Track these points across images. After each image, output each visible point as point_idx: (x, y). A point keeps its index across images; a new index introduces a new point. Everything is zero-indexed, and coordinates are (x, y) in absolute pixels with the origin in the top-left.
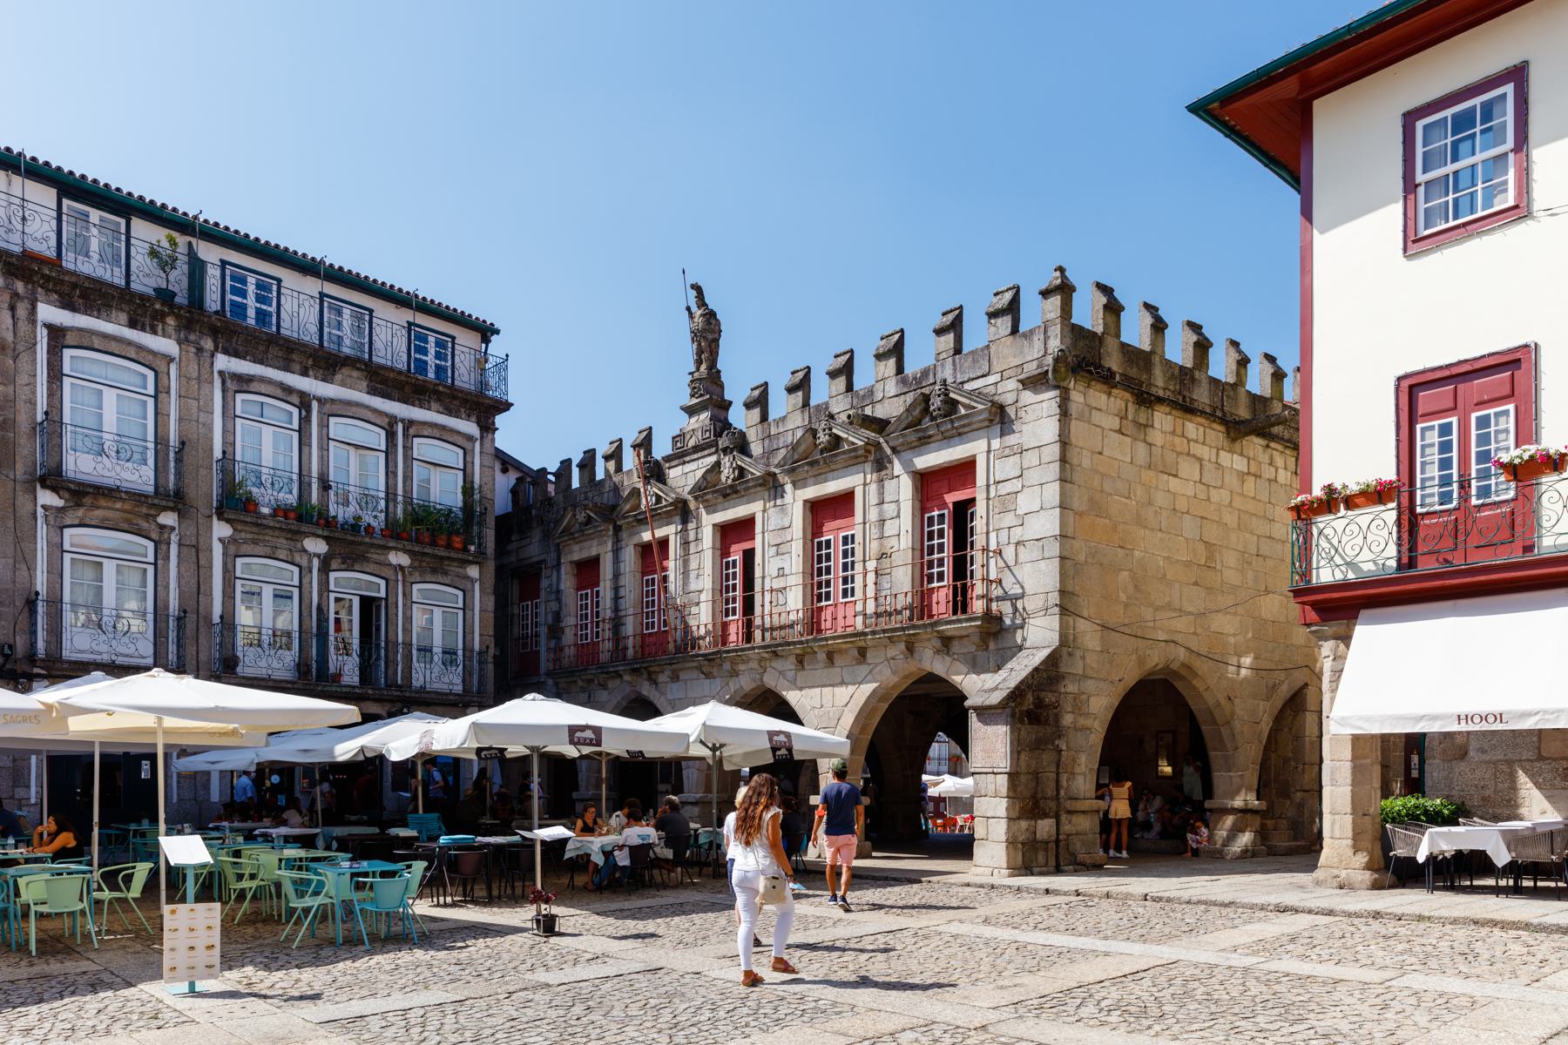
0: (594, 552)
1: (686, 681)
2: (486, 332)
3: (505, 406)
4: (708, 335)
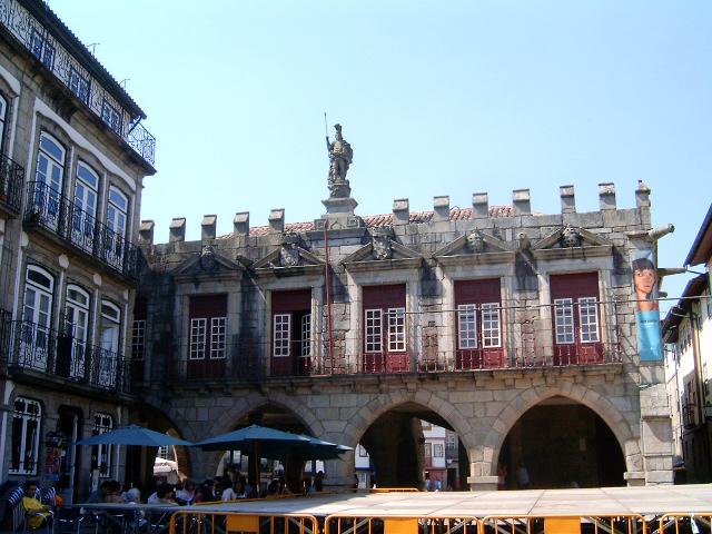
0: (220, 289)
1: (330, 395)
2: (135, 112)
3: (151, 171)
4: (342, 158)
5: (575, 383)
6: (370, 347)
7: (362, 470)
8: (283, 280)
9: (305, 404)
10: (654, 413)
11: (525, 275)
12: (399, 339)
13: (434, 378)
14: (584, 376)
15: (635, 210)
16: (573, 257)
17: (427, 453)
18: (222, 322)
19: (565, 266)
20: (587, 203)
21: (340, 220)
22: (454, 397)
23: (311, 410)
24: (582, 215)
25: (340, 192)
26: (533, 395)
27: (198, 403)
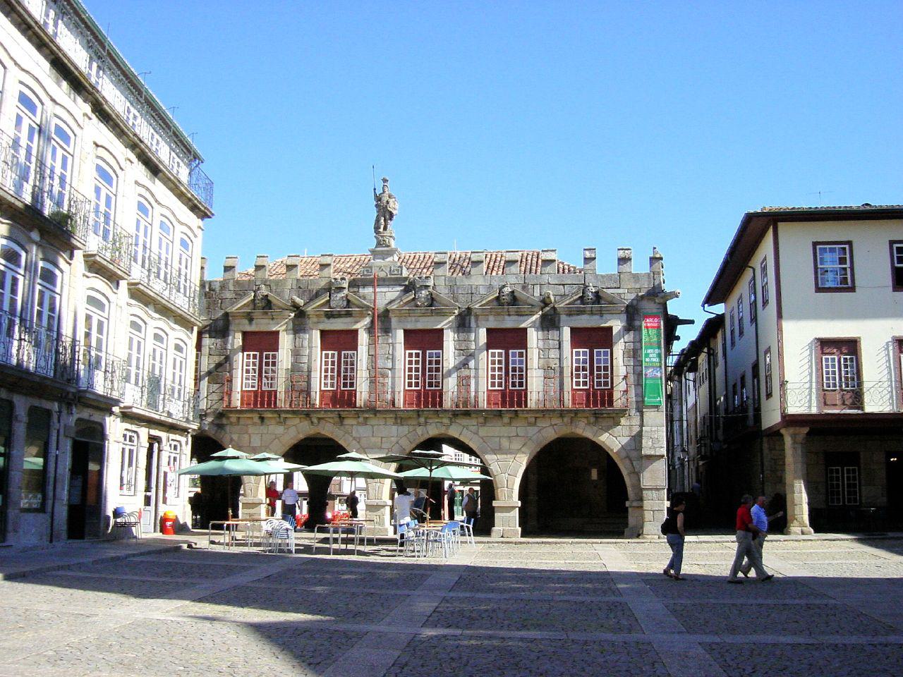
5: (589, 424)
6: (431, 385)
7: (301, 494)
8: (332, 320)
9: (350, 434)
10: (653, 453)
11: (463, 323)
12: (495, 375)
13: (467, 414)
14: (597, 418)
15: (649, 274)
16: (592, 313)
17: (799, 466)
18: (274, 357)
19: (585, 321)
20: (606, 266)
21: (382, 267)
22: (483, 431)
23: (354, 438)
24: (602, 276)
25: (382, 249)
26: (549, 432)
27: (251, 430)
